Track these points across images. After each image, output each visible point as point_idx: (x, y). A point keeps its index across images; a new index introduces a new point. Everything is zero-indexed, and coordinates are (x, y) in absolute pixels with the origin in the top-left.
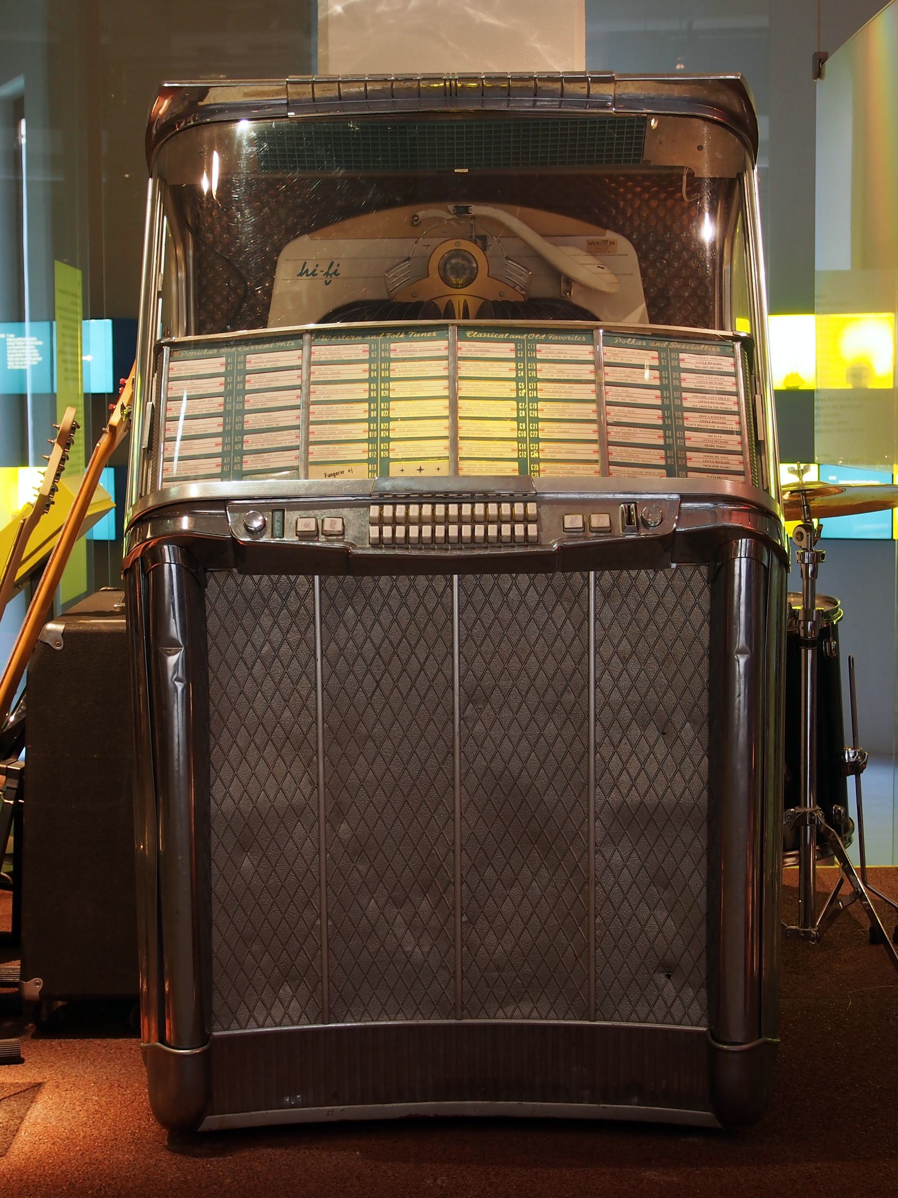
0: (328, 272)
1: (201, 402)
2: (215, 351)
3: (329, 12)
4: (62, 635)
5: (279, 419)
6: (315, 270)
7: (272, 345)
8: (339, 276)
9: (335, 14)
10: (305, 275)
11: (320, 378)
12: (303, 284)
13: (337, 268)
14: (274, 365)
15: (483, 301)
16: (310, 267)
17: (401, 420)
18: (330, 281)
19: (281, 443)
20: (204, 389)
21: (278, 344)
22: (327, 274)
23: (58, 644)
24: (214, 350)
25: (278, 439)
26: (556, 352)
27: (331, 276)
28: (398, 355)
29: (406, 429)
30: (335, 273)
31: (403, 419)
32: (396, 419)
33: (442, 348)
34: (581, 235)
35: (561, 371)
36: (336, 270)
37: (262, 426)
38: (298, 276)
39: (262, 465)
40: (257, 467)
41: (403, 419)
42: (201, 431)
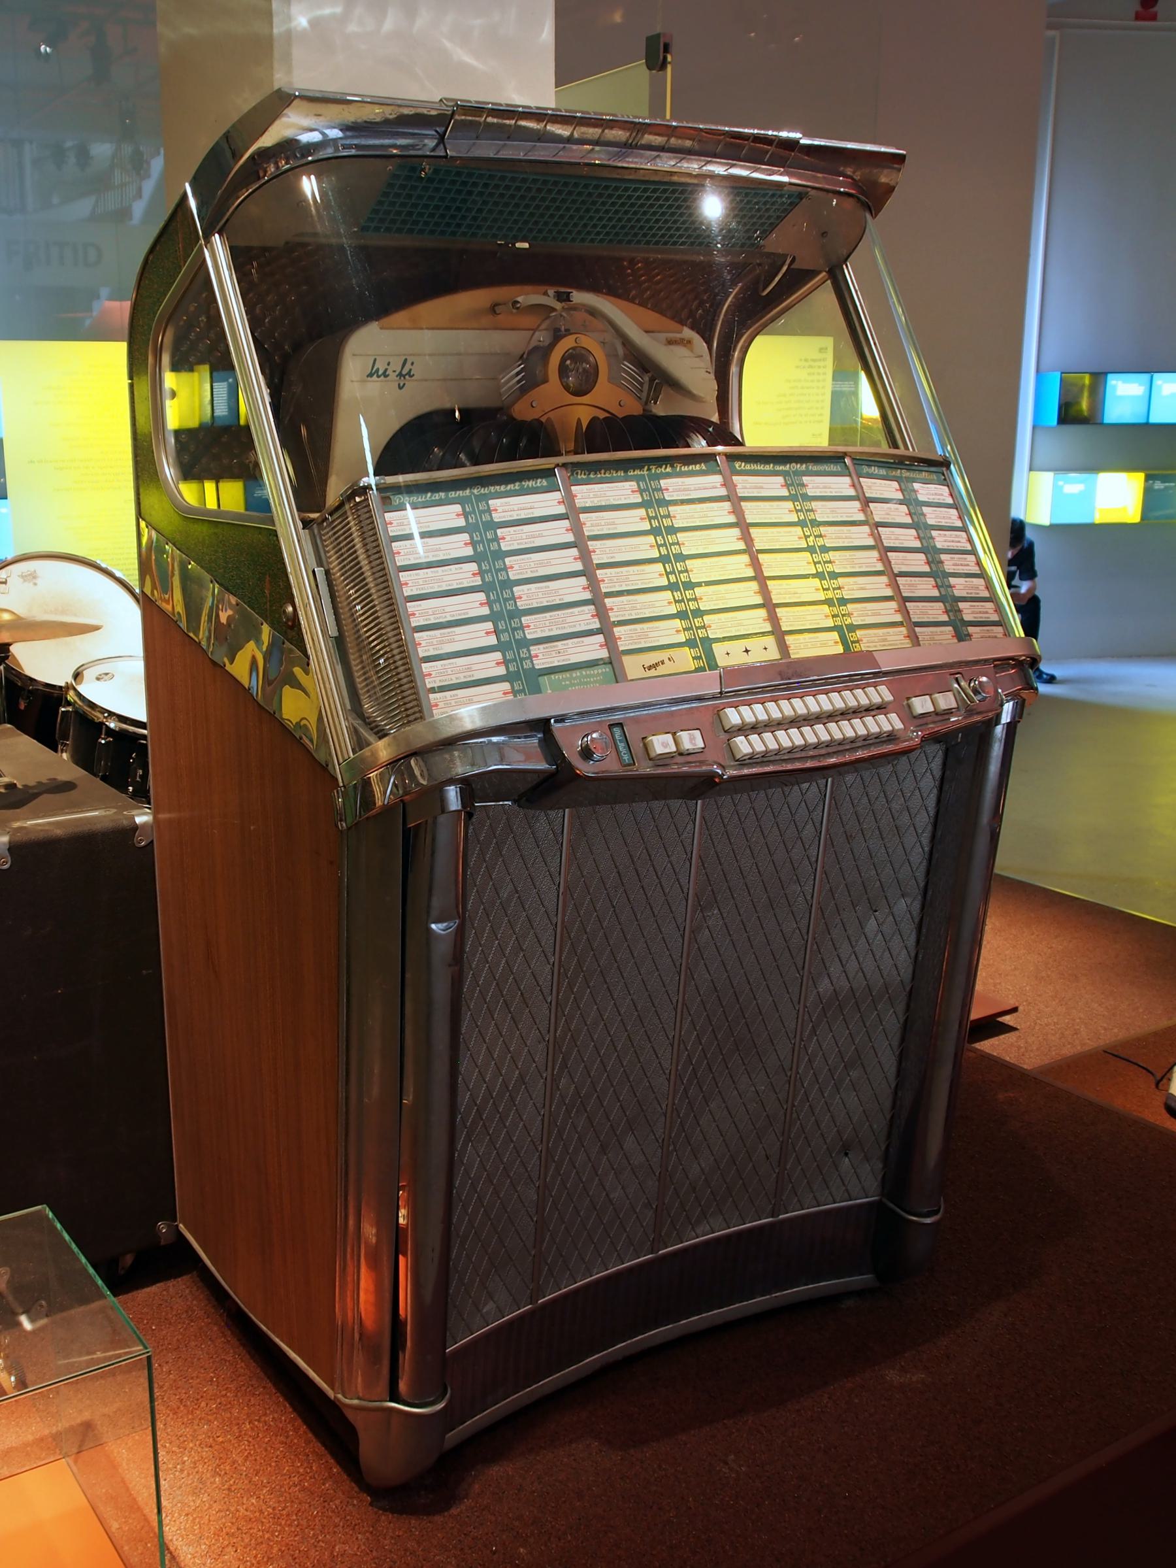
0: (401, 373)
1: (446, 571)
2: (442, 495)
3: (293, 24)
4: (9, 850)
5: (561, 592)
6: (386, 370)
7: (517, 486)
8: (388, 378)
9: (299, 29)
10: (375, 376)
11: (594, 531)
12: (375, 387)
13: (411, 367)
14: (529, 514)
15: (608, 415)
16: (381, 366)
17: (706, 585)
18: (404, 384)
19: (575, 626)
20: (444, 552)
21: (526, 484)
22: (400, 375)
23: (4, 862)
24: (441, 494)
25: (568, 620)
26: (821, 486)
27: (404, 378)
28: (673, 496)
29: (714, 597)
30: (409, 373)
31: (708, 583)
32: (699, 584)
33: (718, 485)
34: (659, 332)
35: (833, 511)
36: (410, 370)
37: (541, 602)
38: (368, 376)
39: (559, 658)
40: (551, 662)
41: (708, 583)
42: (460, 615)
